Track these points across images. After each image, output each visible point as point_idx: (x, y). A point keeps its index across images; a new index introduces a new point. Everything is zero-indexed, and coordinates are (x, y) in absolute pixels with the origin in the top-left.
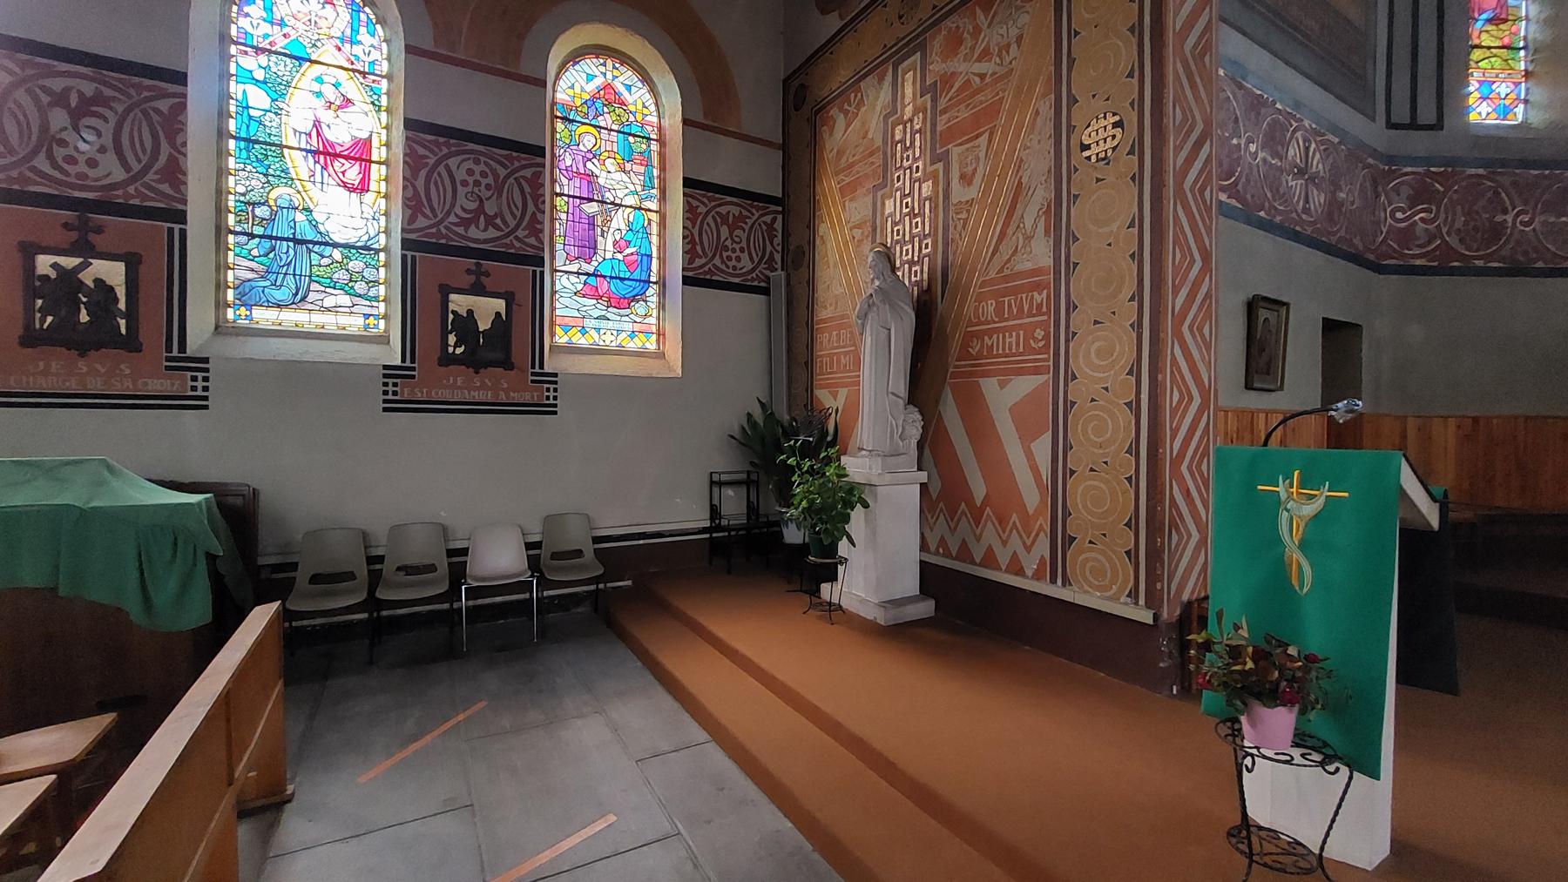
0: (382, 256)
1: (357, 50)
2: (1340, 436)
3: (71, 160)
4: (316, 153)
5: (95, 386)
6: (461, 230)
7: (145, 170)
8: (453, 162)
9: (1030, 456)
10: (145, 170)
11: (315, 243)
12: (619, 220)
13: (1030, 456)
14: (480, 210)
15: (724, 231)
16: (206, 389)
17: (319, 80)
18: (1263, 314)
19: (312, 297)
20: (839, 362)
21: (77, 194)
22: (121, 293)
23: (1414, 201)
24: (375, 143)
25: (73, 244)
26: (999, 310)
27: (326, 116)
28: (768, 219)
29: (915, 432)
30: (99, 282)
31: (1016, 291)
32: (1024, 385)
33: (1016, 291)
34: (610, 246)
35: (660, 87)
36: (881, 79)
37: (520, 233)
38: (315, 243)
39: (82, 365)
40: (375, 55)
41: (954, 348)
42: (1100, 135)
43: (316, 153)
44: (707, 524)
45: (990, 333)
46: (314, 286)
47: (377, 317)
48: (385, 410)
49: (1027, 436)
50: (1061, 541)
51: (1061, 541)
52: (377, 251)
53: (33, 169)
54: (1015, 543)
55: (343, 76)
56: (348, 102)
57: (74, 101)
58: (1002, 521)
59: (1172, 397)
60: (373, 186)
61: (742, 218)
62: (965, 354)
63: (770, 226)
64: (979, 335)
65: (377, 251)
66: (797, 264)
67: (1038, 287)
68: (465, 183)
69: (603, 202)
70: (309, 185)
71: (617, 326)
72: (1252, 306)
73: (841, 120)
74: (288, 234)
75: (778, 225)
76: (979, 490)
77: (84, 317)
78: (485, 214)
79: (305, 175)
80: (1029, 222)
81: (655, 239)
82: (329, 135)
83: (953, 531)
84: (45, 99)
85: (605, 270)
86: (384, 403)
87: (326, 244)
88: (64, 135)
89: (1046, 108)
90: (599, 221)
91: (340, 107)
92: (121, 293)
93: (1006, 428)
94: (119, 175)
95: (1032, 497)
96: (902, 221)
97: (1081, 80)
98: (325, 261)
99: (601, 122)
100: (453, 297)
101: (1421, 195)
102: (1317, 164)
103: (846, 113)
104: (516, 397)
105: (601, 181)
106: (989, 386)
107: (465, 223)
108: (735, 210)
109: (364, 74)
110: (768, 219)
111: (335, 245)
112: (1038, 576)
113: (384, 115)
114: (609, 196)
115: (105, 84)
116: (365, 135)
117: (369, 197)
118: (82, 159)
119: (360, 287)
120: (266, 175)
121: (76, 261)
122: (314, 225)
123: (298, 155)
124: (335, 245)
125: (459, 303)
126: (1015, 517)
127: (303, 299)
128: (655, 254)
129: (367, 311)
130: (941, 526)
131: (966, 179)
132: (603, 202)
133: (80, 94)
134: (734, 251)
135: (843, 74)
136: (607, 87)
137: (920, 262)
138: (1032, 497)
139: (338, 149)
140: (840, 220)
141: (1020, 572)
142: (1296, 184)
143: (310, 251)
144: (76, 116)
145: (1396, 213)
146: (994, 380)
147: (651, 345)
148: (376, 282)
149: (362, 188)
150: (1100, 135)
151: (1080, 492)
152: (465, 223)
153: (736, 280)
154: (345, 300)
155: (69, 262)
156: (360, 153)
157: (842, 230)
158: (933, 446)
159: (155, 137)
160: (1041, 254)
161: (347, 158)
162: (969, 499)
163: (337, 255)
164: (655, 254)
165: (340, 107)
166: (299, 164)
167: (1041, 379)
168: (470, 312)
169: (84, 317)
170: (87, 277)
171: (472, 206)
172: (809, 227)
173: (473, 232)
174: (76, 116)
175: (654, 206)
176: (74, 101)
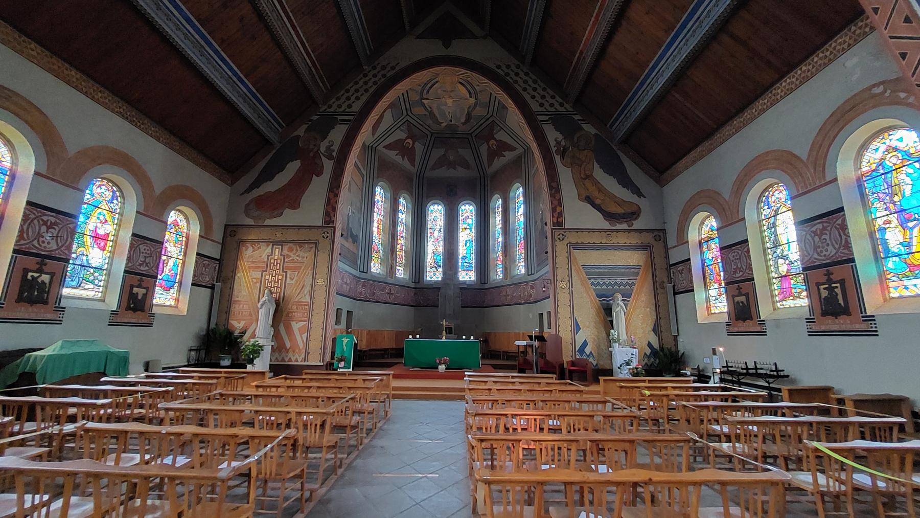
0: (105, 271)
1: (112, 205)
2: (348, 333)
3: (43, 242)
4: (93, 237)
5: (33, 316)
6: (139, 267)
7: (62, 246)
8: (141, 246)
9: (302, 337)
10: (62, 246)
11: (87, 267)
12: (171, 262)
13: (302, 337)
14: (144, 261)
15: (204, 268)
16: (62, 317)
17: (99, 214)
18: (339, 311)
19: (82, 285)
20: (242, 313)
21: (43, 253)
22: (47, 285)
23: (362, 287)
24: (110, 235)
25: (37, 269)
26: (297, 308)
27: (99, 225)
28: (215, 265)
29: (272, 333)
30: (43, 282)
31: (301, 305)
32: (301, 324)
33: (301, 305)
34: (167, 271)
35: (191, 222)
36: (268, 246)
37: (153, 269)
38: (87, 267)
39: (30, 309)
40: (116, 207)
41: (284, 315)
42: (320, 282)
43: (93, 237)
44: (186, 364)
45: (292, 313)
46: (84, 281)
47: (99, 292)
48: (109, 325)
49: (301, 333)
50: (307, 353)
51: (307, 353)
52: (104, 270)
53: (33, 245)
54: (297, 356)
55: (106, 212)
56: (106, 221)
57: (49, 224)
58: (294, 352)
59: (328, 327)
60: (107, 249)
61: (209, 265)
62: (287, 316)
63: (215, 268)
64: (292, 313)
65: (104, 270)
66: (224, 281)
67: (307, 305)
68: (143, 253)
69: (167, 256)
70: (90, 247)
71: (165, 297)
72: (337, 309)
73: (251, 249)
74: (80, 263)
75: (217, 268)
76: (288, 345)
77: (36, 293)
78: (47, 226)
79: (89, 244)
80: (305, 292)
81: (179, 268)
82: (99, 232)
83: (280, 356)
84: (41, 223)
85: (165, 278)
86: (452, 333)
87: (90, 267)
88: (43, 234)
89: (311, 272)
90: (166, 262)
91: (104, 223)
92: (47, 285)
93: (296, 332)
94: (55, 247)
95: (301, 345)
96: (271, 282)
97: (318, 270)
98: (88, 273)
99: (171, 231)
100: (134, 288)
101: (364, 286)
102: (348, 282)
103: (253, 248)
104: (143, 321)
105: (168, 249)
106: (293, 323)
107: (140, 265)
108: (207, 262)
109: (112, 212)
110: (215, 265)
111: (92, 268)
112: (301, 361)
113: (115, 226)
114: (170, 254)
115: (58, 219)
116: (108, 232)
117: (105, 252)
118: (46, 242)
119: (96, 282)
120: (78, 243)
121: (38, 275)
122: (87, 260)
123: (88, 237)
124: (92, 268)
125: (135, 290)
126: (297, 351)
127: (79, 286)
128: (179, 273)
129: (97, 290)
130: (277, 355)
131: (292, 279)
132: (167, 256)
133: (51, 222)
134: (146, 253)
135: (252, 237)
136: (176, 220)
137: (276, 293)
138: (301, 345)
139: (100, 237)
140: (247, 276)
141: (298, 361)
142: (345, 286)
143: (85, 269)
144: (48, 228)
145: (360, 289)
146: (294, 322)
147: (173, 303)
148: (101, 280)
149: (103, 249)
150: (320, 282)
151: (311, 345)
152: (140, 265)
153: (204, 284)
154: (91, 286)
155: (36, 275)
156: (105, 238)
157: (248, 278)
158: (277, 336)
159: (67, 235)
160: (307, 299)
161: (102, 239)
162: (285, 348)
163: (92, 271)
164: (179, 273)
165: (104, 223)
166: (88, 240)
167: (305, 323)
168: (137, 293)
169: (36, 293)
170: (39, 280)
171: (143, 260)
172: (233, 272)
173: (142, 268)
174: (48, 228)
175: (181, 257)
176: (49, 224)
